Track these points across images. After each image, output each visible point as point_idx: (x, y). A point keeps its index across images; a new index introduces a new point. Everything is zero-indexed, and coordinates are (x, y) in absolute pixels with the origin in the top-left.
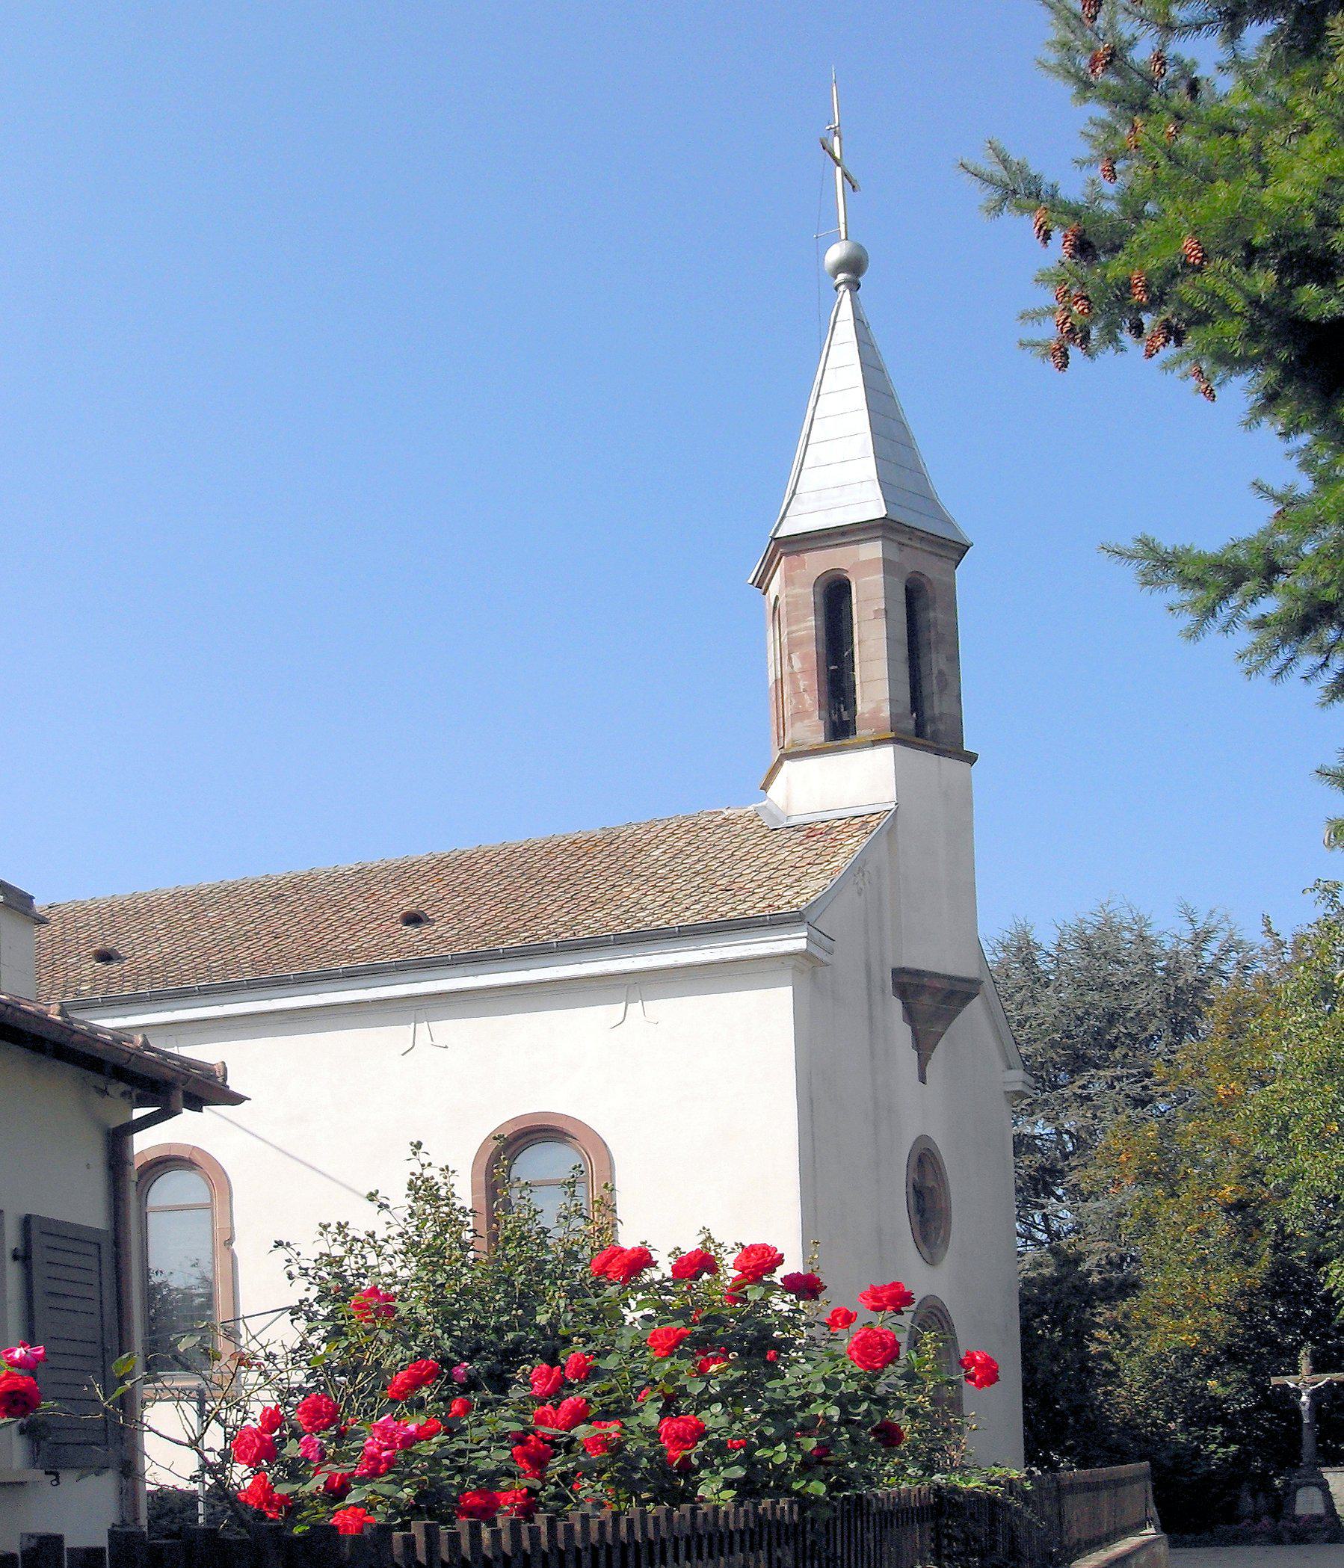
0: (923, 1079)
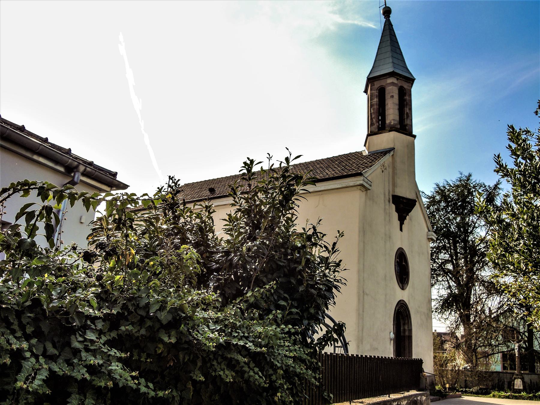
0: (401, 230)
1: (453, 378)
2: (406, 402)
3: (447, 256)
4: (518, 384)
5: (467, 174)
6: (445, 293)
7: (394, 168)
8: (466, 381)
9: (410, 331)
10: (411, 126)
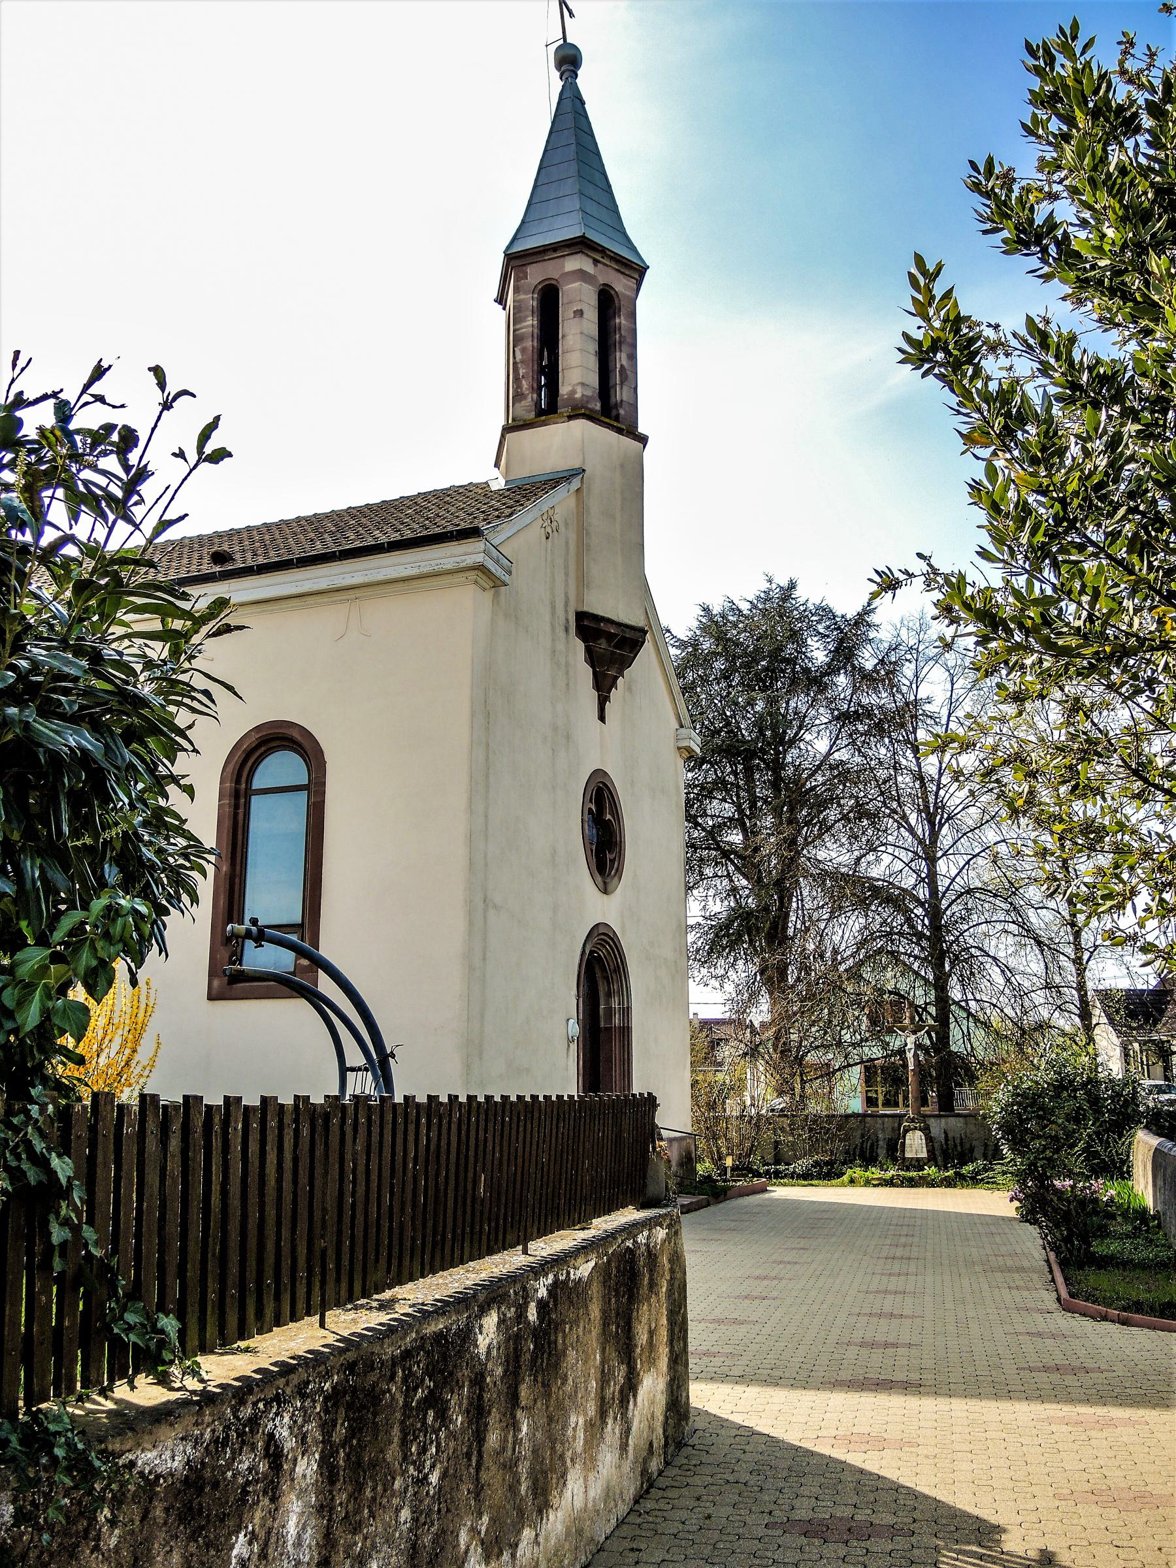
0: (602, 718)
1: (743, 1138)
2: (592, 1264)
3: (729, 810)
4: (915, 1144)
5: (784, 583)
6: (718, 907)
7: (582, 531)
8: (777, 1143)
9: (626, 1012)
10: (634, 407)
